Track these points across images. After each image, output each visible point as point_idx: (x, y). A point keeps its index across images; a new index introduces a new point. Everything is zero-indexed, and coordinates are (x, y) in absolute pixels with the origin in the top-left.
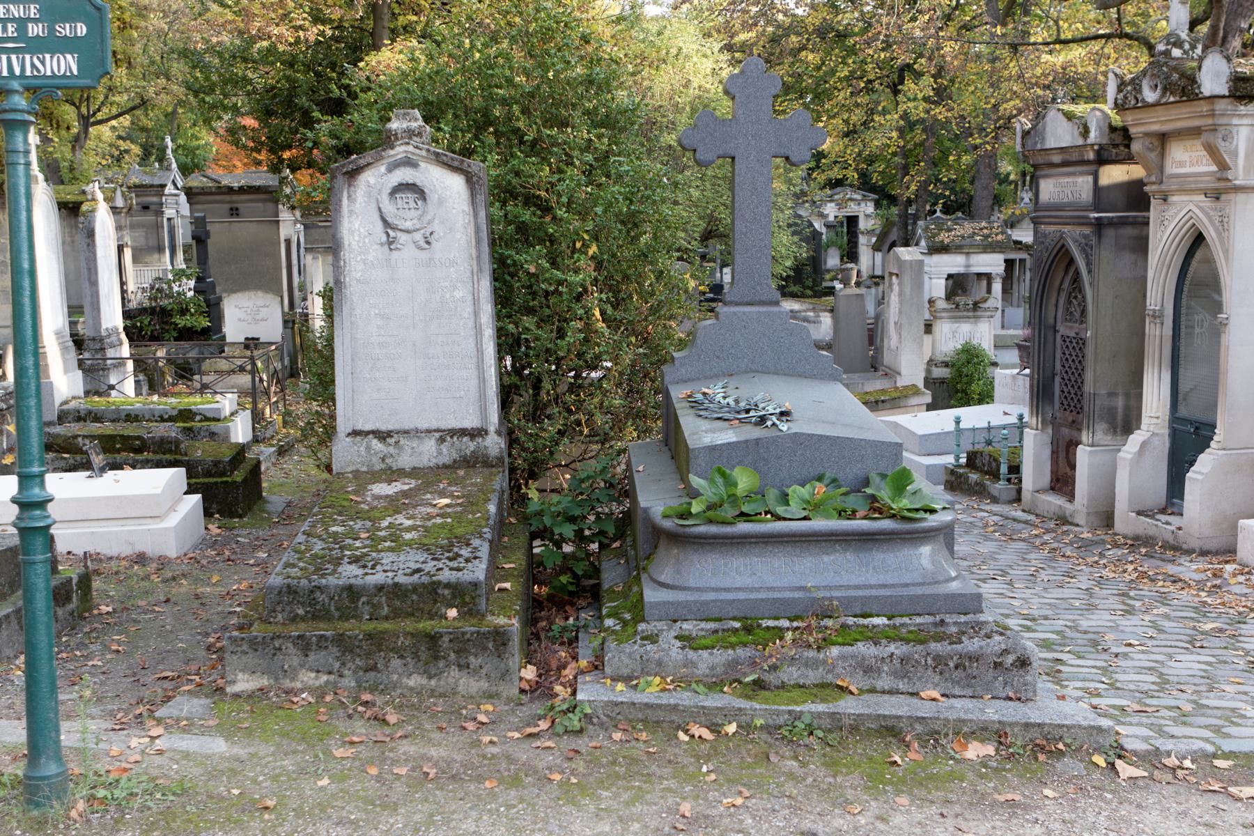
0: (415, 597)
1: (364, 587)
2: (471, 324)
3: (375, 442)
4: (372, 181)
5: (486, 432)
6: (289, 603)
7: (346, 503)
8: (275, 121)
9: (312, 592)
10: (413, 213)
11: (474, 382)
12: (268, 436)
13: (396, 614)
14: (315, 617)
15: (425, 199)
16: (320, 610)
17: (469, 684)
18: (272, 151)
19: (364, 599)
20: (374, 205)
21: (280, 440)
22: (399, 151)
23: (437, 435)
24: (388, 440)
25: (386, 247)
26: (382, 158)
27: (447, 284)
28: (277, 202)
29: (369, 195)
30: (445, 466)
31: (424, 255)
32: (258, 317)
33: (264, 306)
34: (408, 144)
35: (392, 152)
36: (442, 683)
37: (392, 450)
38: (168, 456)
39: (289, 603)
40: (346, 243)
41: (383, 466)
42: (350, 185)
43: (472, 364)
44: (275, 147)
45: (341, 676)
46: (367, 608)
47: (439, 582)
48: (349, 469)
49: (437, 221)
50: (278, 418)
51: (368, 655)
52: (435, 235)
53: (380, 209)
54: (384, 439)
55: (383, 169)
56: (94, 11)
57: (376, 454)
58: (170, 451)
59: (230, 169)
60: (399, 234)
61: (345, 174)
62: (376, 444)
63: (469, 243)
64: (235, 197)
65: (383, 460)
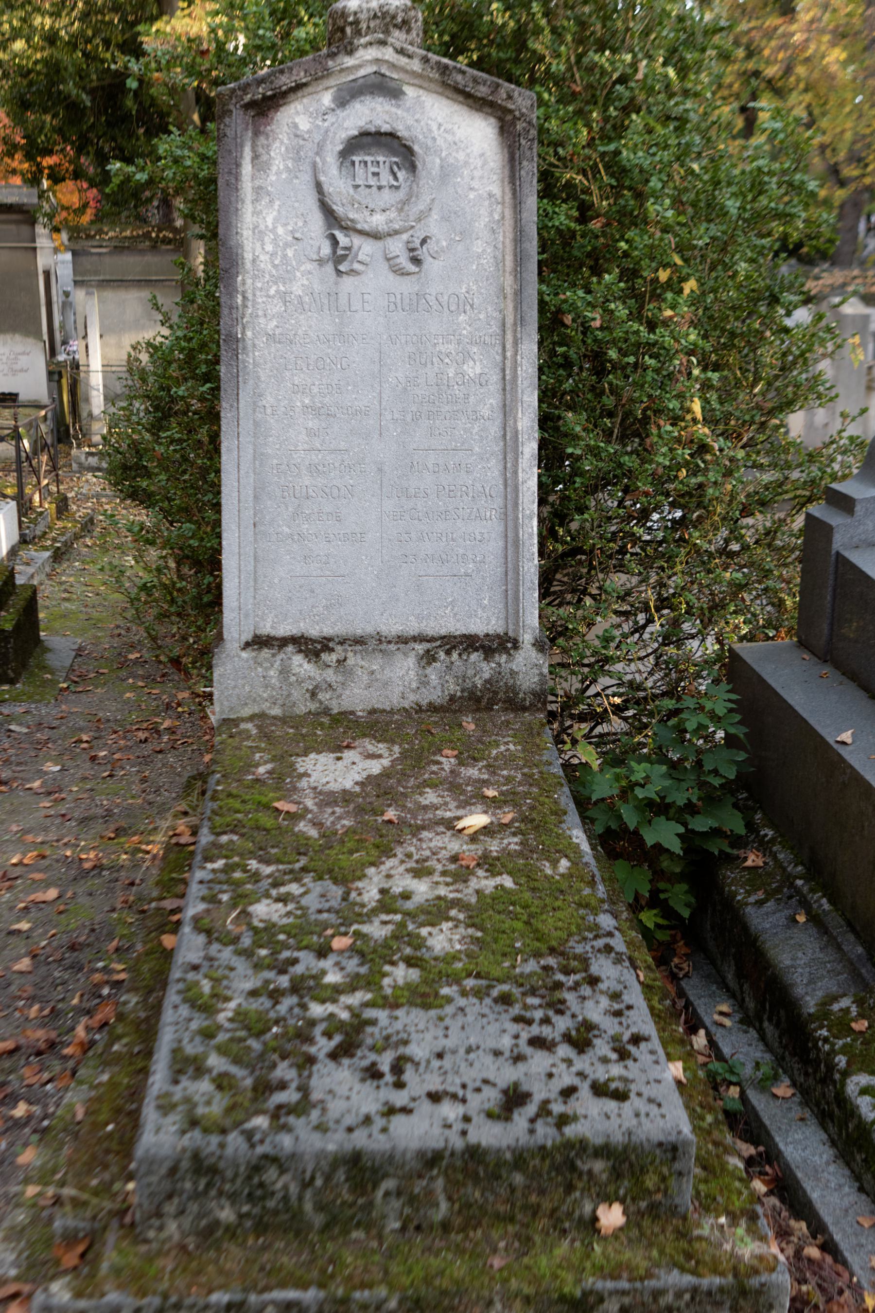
0: (518, 1179)
2: (495, 429)
3: (298, 660)
4: (304, 124)
6: (196, 1196)
7: (266, 820)
9: (256, 1169)
10: (387, 197)
11: (495, 545)
12: (38, 533)
15: (412, 168)
16: (276, 1212)
18: (29, 156)
20: (305, 180)
21: (54, 540)
22: (365, 59)
23: (420, 648)
24: (324, 656)
25: (329, 268)
26: (327, 73)
27: (451, 348)
28: (33, 222)
29: (296, 154)
30: (433, 708)
31: (406, 287)
32: (18, 367)
33: (24, 353)
34: (383, 43)
35: (349, 61)
37: (330, 675)
39: (196, 1196)
40: (248, 256)
41: (313, 706)
42: (257, 133)
43: (492, 508)
46: (396, 1204)
47: (581, 1146)
48: (246, 712)
49: (435, 215)
50: (49, 507)
52: (431, 245)
53: (319, 187)
54: (317, 654)
55: (327, 99)
57: (299, 682)
60: (357, 240)
61: (248, 106)
62: (301, 665)
63: (499, 263)
65: (313, 694)
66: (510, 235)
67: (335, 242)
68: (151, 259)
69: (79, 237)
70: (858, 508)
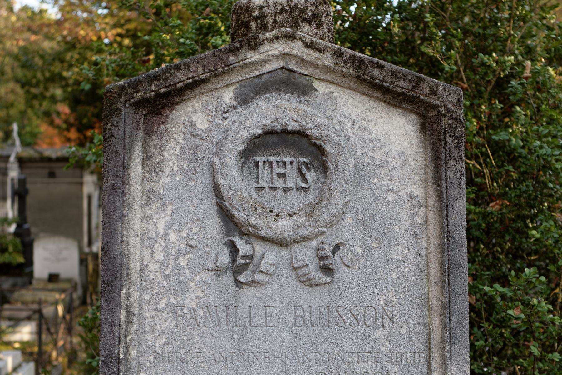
4: (202, 122)
8: (80, 108)
10: (295, 200)
15: (324, 168)
20: (204, 179)
22: (271, 53)
25: (228, 278)
26: (228, 69)
29: (193, 155)
31: (315, 298)
34: (291, 37)
35: (253, 57)
40: (135, 266)
42: (149, 133)
44: (82, 128)
49: (349, 220)
53: (217, 189)
55: (228, 96)
59: (51, 144)
60: (259, 248)
61: (138, 105)
63: (423, 271)
64: (53, 165)
66: (435, 241)
67: (234, 250)
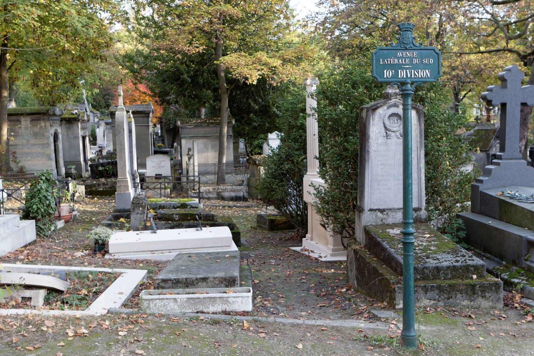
0: (461, 271)
1: (442, 267)
3: (379, 213)
4: (381, 112)
5: (421, 209)
9: (423, 269)
13: (453, 277)
14: (424, 279)
17: (485, 304)
19: (442, 272)
20: (382, 122)
22: (393, 101)
26: (386, 103)
29: (380, 118)
35: (390, 101)
36: (475, 303)
37: (385, 216)
38: (209, 222)
41: (382, 223)
45: (439, 301)
46: (443, 275)
51: (449, 293)
53: (384, 123)
55: (385, 108)
56: (435, 54)
58: (210, 220)
62: (379, 214)
65: (382, 220)
66: (419, 131)
67: (387, 133)
68: (207, 129)
69: (183, 123)
70: (484, 182)
